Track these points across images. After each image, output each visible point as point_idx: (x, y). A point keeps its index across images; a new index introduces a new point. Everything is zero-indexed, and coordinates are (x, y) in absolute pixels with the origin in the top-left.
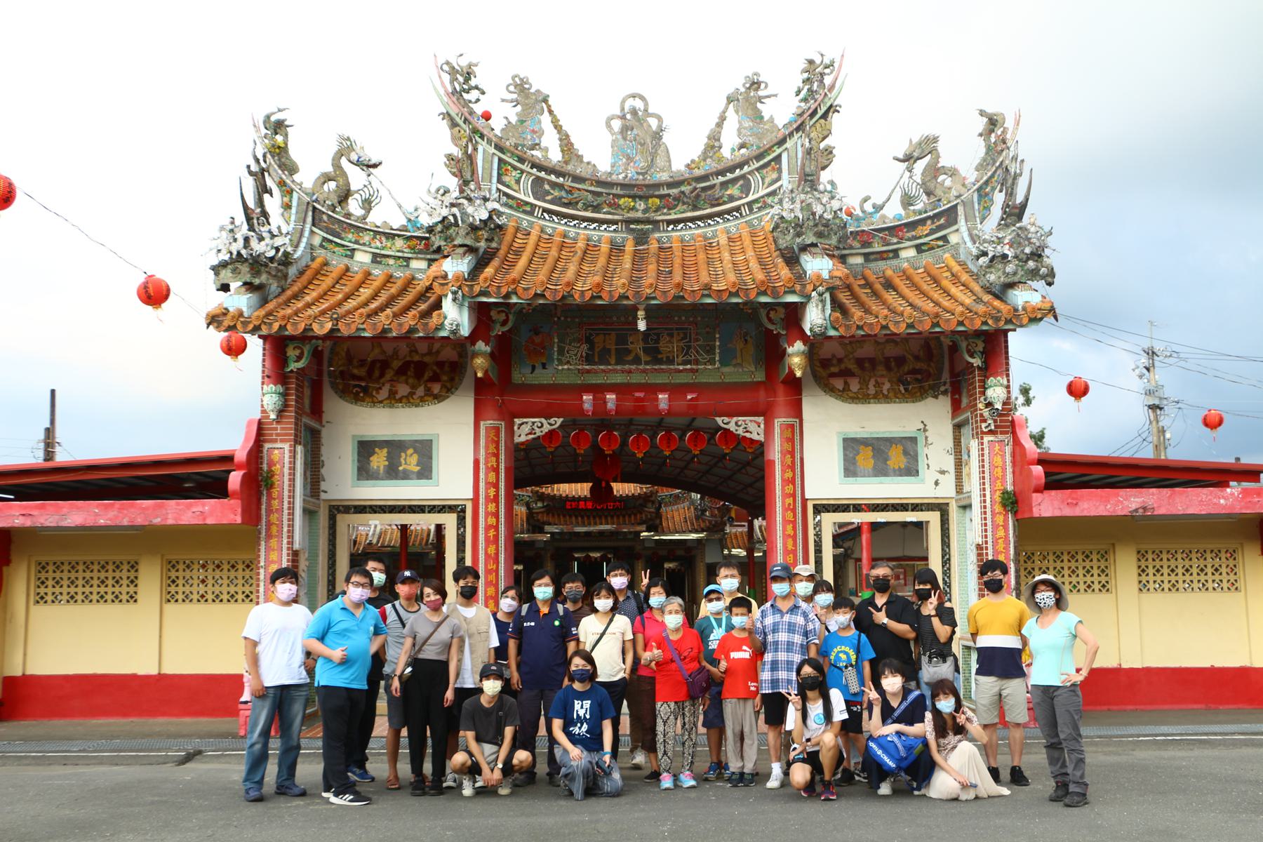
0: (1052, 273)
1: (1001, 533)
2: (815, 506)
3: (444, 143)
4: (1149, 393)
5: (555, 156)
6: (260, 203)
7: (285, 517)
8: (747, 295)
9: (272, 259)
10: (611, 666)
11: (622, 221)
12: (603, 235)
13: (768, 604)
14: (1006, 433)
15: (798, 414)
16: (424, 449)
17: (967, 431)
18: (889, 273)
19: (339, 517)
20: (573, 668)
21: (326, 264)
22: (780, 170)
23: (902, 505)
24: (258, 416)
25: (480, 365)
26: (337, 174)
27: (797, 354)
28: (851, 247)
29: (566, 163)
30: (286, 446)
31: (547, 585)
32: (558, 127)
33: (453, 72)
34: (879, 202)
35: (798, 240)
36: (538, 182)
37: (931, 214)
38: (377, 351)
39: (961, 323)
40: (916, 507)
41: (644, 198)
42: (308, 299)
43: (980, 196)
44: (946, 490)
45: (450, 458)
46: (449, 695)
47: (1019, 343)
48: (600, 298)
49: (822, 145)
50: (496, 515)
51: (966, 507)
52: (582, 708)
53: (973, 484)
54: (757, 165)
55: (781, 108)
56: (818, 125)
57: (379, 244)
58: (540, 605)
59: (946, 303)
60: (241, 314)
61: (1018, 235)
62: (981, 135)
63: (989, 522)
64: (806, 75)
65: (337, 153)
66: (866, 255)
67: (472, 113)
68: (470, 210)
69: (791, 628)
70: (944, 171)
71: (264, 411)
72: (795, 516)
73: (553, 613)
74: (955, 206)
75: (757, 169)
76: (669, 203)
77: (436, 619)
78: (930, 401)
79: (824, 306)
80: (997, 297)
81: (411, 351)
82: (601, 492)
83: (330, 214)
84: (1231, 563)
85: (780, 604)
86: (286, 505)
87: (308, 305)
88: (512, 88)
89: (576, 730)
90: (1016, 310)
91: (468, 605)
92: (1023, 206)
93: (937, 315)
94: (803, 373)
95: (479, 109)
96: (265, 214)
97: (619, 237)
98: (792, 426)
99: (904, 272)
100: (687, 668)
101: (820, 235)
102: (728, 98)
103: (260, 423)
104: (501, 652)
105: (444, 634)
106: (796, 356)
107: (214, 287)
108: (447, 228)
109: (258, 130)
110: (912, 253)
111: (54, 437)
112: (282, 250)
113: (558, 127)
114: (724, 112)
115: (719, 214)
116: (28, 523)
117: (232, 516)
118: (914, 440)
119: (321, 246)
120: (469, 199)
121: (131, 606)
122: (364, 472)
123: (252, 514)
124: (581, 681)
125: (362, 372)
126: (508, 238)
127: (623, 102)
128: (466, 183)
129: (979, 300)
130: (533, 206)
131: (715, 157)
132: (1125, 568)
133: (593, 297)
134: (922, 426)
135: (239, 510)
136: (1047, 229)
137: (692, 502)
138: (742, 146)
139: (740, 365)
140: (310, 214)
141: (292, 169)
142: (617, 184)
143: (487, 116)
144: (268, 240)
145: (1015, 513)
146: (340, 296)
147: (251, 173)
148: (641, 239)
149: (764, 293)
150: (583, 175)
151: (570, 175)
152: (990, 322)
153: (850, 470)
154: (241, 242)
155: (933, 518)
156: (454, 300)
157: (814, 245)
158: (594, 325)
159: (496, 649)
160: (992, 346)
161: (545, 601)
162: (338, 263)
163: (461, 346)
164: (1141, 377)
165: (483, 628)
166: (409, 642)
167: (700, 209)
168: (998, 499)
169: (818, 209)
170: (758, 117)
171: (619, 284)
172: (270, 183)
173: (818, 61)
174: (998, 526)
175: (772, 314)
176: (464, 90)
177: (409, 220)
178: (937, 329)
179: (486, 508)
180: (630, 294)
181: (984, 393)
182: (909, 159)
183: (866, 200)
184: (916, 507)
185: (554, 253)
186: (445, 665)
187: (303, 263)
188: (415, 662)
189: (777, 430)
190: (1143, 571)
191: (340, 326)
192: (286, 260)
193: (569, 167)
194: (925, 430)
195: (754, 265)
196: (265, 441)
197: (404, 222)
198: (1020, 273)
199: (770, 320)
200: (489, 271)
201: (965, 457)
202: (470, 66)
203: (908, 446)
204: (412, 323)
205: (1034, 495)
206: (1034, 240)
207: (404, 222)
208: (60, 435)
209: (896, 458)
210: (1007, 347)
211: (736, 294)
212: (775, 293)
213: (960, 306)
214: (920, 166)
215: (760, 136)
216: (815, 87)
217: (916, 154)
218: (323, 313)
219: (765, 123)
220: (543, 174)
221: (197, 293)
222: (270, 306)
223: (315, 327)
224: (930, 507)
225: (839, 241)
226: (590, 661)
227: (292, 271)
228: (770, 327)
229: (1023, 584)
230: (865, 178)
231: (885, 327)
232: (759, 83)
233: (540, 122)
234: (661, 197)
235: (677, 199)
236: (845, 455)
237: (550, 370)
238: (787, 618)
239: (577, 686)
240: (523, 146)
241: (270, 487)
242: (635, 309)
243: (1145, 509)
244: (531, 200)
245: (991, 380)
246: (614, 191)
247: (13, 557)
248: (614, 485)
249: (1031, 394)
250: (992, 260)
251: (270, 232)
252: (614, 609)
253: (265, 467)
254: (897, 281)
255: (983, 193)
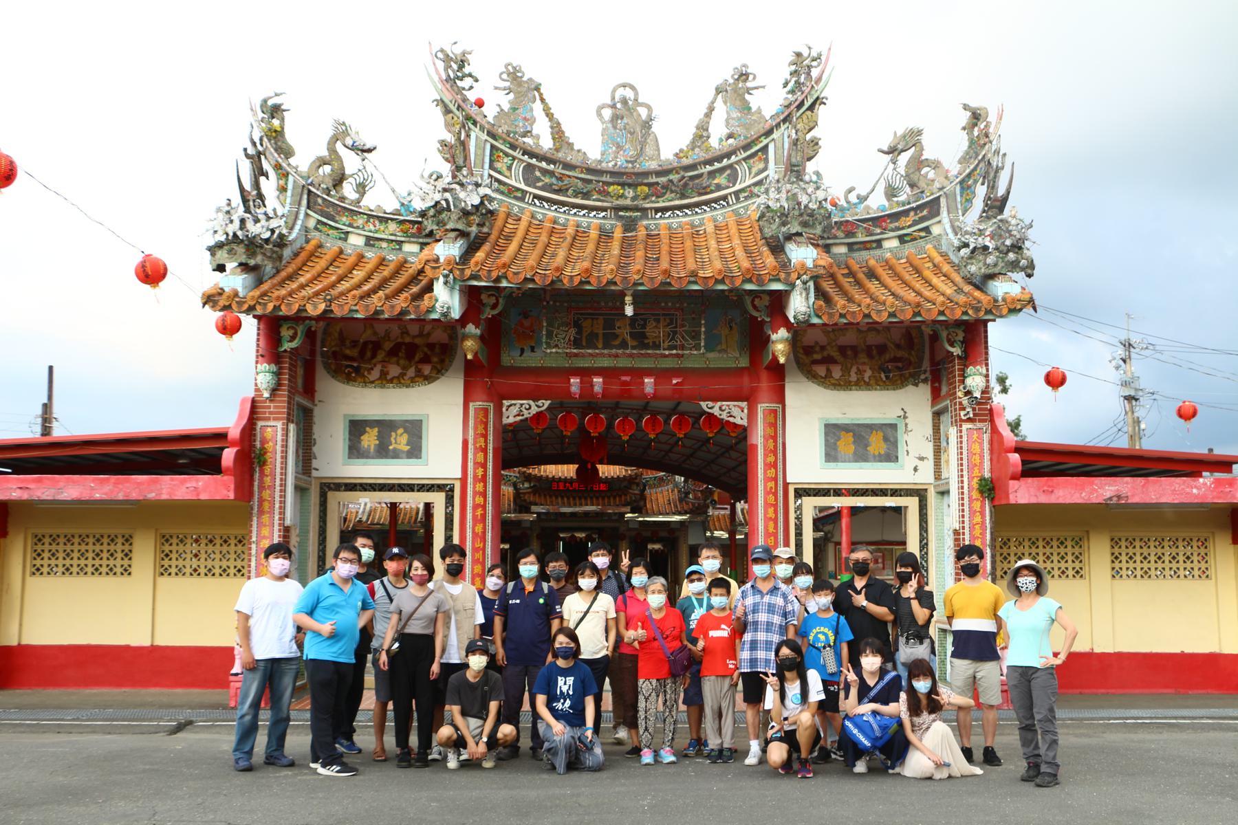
0: (1031, 265)
1: (978, 519)
2: (796, 490)
3: (437, 129)
4: (1125, 384)
5: (546, 143)
6: (257, 185)
7: (277, 494)
8: (732, 283)
9: (267, 241)
10: (594, 643)
11: (611, 208)
12: (593, 221)
13: (748, 585)
14: (984, 421)
15: (781, 399)
16: (415, 429)
17: (946, 419)
18: (872, 262)
19: (330, 494)
20: (557, 645)
21: (320, 246)
22: (766, 161)
23: (881, 490)
24: (252, 394)
25: (470, 347)
26: (332, 158)
27: (781, 341)
28: (835, 237)
29: (557, 150)
30: (279, 425)
31: (532, 563)
32: (549, 115)
33: (447, 59)
34: (864, 193)
35: (784, 229)
36: (529, 168)
37: (914, 205)
38: (369, 332)
39: (942, 313)
40: (895, 493)
41: (633, 186)
42: (302, 280)
43: (962, 188)
44: (925, 476)
45: (439, 438)
46: (435, 668)
47: (997, 332)
48: (589, 283)
49: (808, 137)
50: (484, 495)
51: (944, 493)
52: (565, 684)
53: (951, 471)
54: (744, 155)
55: (769, 100)
56: (804, 117)
57: (372, 227)
58: (525, 583)
59: (927, 293)
60: (236, 294)
61: (999, 227)
62: (964, 128)
63: (966, 508)
64: (793, 68)
65: (332, 138)
66: (850, 245)
67: (465, 100)
68: (462, 195)
69: (771, 609)
70: (927, 163)
71: (257, 390)
72: (776, 499)
73: (538, 591)
74: (938, 198)
75: (745, 159)
76: (658, 191)
77: (421, 594)
78: (911, 388)
79: (808, 294)
80: (978, 288)
81: (402, 333)
82: (587, 473)
83: (325, 197)
84: (1203, 551)
85: (760, 585)
86: (278, 482)
87: (302, 287)
88: (505, 76)
89: (559, 706)
90: (996, 301)
91: (454, 582)
92: (1004, 200)
93: (918, 305)
94: (787, 360)
95: (472, 96)
96: (260, 196)
97: (608, 224)
98: (775, 412)
99: (887, 262)
100: (669, 647)
101: (805, 224)
102: (717, 89)
103: (253, 401)
104: (486, 628)
105: (428, 608)
106: (779, 342)
107: (210, 268)
108: (440, 212)
109: (255, 114)
110: (895, 243)
111: (51, 413)
112: (277, 232)
113: (549, 115)
114: (713, 103)
115: (706, 203)
116: (25, 496)
117: (225, 492)
118: (894, 427)
119: (316, 228)
120: (462, 185)
121: (125, 578)
122: (355, 451)
123: (245, 489)
124: (565, 658)
125: (354, 353)
126: (499, 223)
127: (614, 91)
128: (459, 169)
129: (959, 290)
130: (524, 192)
131: (703, 147)
132: (1099, 555)
133: (581, 282)
134: (902, 413)
135: (232, 486)
136: (1027, 222)
137: (676, 485)
138: (730, 136)
139: (725, 351)
140: (305, 197)
141: (288, 152)
142: (606, 172)
143: (480, 103)
144: (263, 222)
145: (992, 500)
146: (334, 278)
147: (247, 156)
148: (630, 226)
149: (750, 281)
150: (574, 162)
151: (560, 162)
152: (970, 312)
153: (831, 456)
154: (237, 224)
155: (912, 503)
156: (446, 283)
157: (799, 234)
158: (582, 310)
159: (481, 625)
160: (972, 335)
161: (530, 579)
162: (332, 245)
163: (452, 328)
164: (1117, 368)
165: (469, 605)
166: (395, 617)
167: (688, 197)
168: (975, 486)
169: (804, 199)
170: (746, 108)
171: (608, 270)
172: (266, 166)
173: (805, 54)
174: (975, 511)
175: (757, 302)
176: (458, 78)
177: (403, 204)
178: (919, 319)
179: (474, 487)
180: (618, 279)
181: (963, 377)
182: (893, 151)
183: (850, 190)
184: (895, 493)
185: (544, 238)
186: (429, 640)
187: (298, 245)
188: (402, 637)
189: (760, 415)
190: (1117, 558)
191: (334, 307)
192: (281, 242)
193: (560, 155)
194: (905, 417)
195: (740, 253)
196: (259, 419)
197: (398, 206)
198: (1001, 264)
199: (755, 307)
200: (480, 255)
201: (944, 444)
202: (464, 54)
203: (889, 432)
204: (404, 305)
205: (1011, 482)
206: (1014, 233)
207: (398, 206)
208: (57, 411)
209: (876, 444)
210: (986, 337)
211: (722, 281)
212: (760, 280)
213: (942, 296)
214: (904, 158)
215: (747, 127)
216: (802, 80)
217: (900, 147)
218: (317, 294)
219: (753, 114)
220: (534, 161)
221: (194, 273)
222: (265, 287)
223: (309, 308)
224: (909, 492)
225: (824, 231)
226: (573, 637)
227: (287, 253)
228: (755, 314)
229: (999, 569)
230: (849, 169)
231: (868, 316)
232: (747, 75)
233: (532, 110)
234: (649, 185)
235: (665, 187)
236: (826, 440)
237: (538, 354)
238: (767, 599)
239: (561, 663)
240: (515, 133)
241: (263, 464)
242: (622, 294)
243: (1119, 497)
244: (522, 186)
245: (971, 369)
246: (604, 179)
247: (11, 529)
248: (599, 467)
249: (1008, 383)
250: (973, 251)
251: (265, 214)
252: (598, 588)
253: (258, 444)
254: (880, 271)
255: (966, 185)
